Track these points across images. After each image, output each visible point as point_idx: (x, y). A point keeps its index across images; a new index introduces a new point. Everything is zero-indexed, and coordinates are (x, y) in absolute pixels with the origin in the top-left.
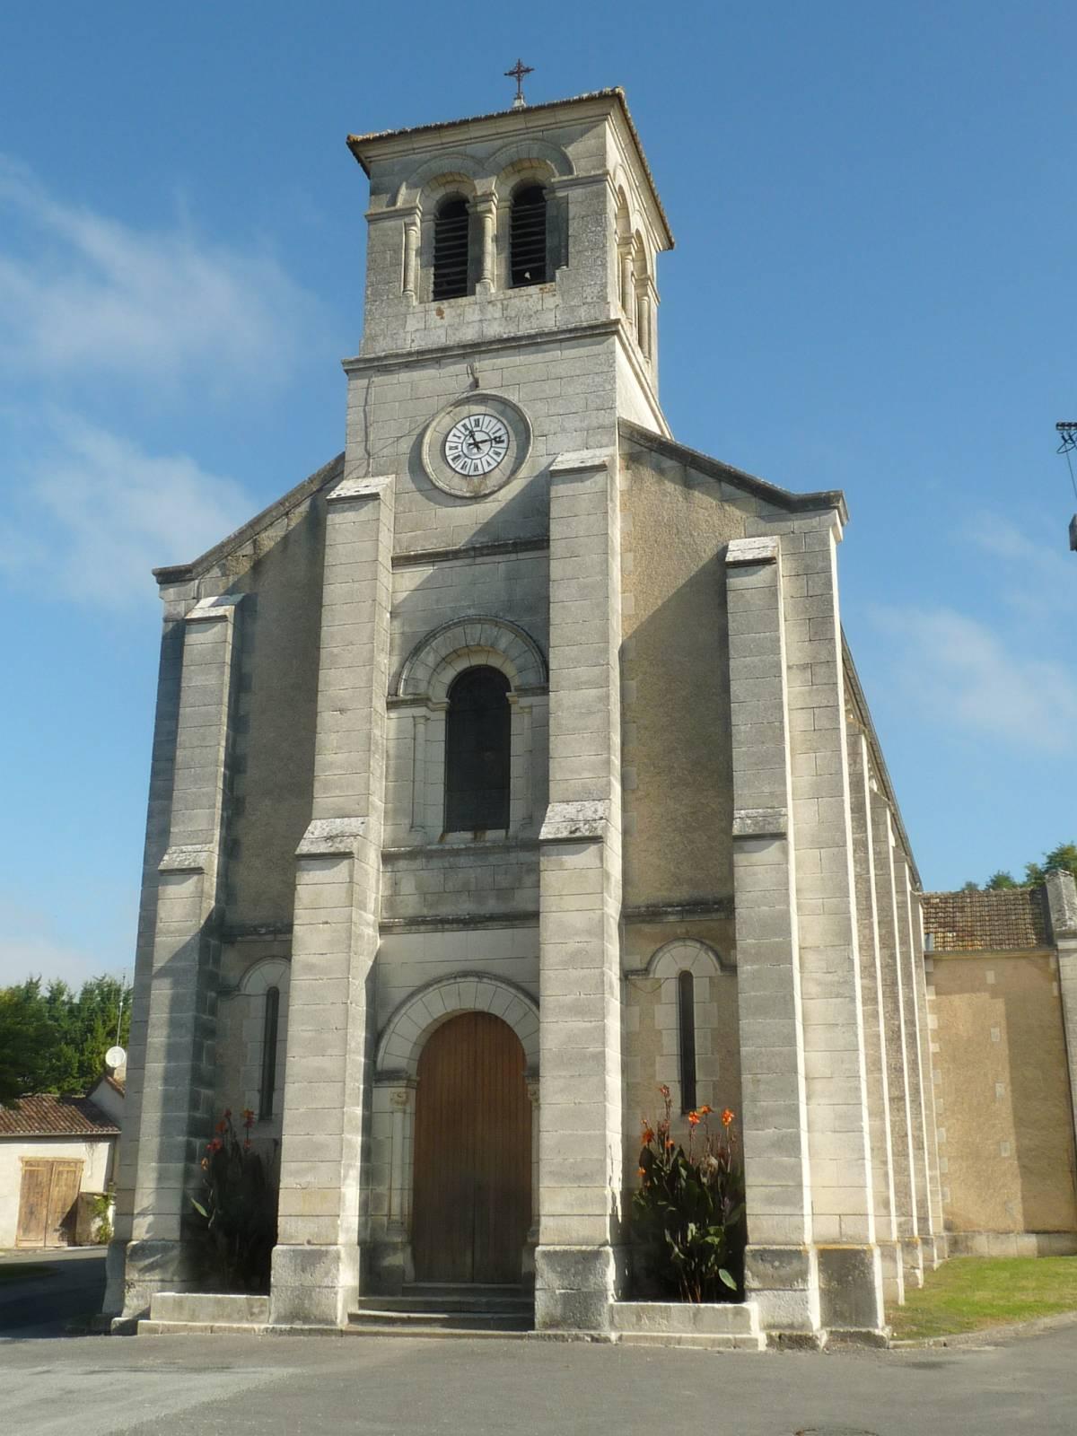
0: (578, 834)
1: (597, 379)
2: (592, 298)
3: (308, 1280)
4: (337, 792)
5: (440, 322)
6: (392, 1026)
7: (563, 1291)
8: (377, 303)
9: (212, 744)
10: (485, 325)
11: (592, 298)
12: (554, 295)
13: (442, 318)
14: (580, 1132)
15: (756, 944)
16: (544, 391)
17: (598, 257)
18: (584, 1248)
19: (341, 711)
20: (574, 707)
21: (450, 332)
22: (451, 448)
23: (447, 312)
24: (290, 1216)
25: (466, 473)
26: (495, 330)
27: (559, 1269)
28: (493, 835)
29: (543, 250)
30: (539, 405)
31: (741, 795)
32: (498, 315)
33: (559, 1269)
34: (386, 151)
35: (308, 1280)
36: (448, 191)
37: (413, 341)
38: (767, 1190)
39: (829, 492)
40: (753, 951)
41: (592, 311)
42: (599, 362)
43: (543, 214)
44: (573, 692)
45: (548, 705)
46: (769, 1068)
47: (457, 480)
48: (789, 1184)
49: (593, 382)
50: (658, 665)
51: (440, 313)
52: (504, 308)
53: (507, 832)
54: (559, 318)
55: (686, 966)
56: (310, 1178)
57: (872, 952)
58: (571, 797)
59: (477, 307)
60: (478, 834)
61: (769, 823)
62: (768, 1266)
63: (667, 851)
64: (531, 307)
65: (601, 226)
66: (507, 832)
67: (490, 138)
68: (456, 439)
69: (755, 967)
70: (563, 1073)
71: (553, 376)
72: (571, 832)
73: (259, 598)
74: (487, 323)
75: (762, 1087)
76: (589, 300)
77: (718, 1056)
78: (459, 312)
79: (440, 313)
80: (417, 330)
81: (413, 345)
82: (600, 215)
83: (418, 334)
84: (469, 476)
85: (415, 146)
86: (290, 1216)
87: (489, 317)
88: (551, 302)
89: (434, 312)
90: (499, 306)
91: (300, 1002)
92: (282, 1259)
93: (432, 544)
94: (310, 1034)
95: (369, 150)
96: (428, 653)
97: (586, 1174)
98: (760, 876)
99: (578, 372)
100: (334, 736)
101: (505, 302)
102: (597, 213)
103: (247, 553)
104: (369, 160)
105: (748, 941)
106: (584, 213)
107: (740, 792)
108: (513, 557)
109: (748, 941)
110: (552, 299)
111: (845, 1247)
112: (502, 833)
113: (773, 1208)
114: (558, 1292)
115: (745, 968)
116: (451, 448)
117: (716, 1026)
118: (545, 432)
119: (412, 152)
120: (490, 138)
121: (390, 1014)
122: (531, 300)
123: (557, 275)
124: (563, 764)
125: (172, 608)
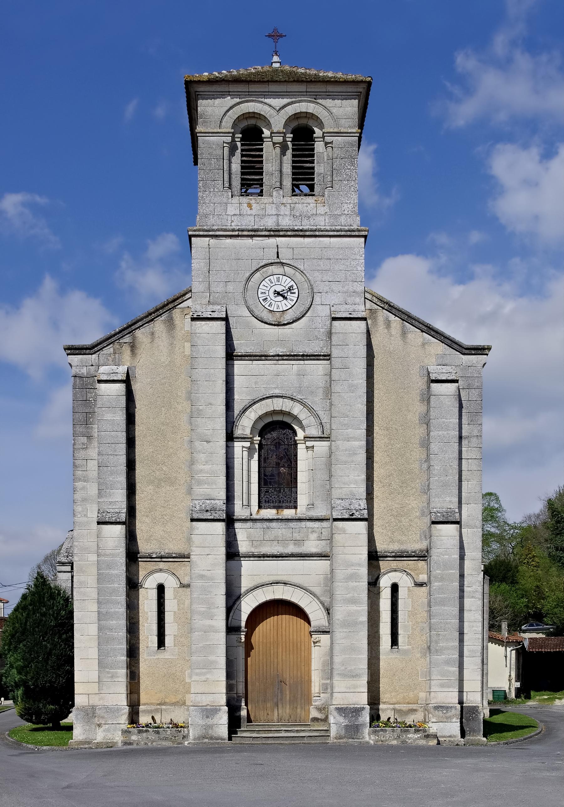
0: (354, 517)
1: (352, 263)
2: (348, 211)
3: (210, 721)
4: (206, 486)
5: (249, 212)
6: (236, 606)
7: (345, 724)
8: (207, 193)
9: (120, 454)
10: (280, 218)
11: (348, 211)
12: (324, 206)
13: (251, 209)
14: (354, 656)
15: (441, 573)
16: (319, 265)
17: (352, 186)
18: (356, 706)
19: (208, 442)
20: (346, 450)
21: (257, 219)
22: (262, 293)
23: (254, 206)
24: (198, 693)
25: (271, 309)
26: (286, 223)
27: (344, 715)
28: (288, 513)
29: (313, 174)
30: (317, 274)
31: (433, 501)
32: (288, 213)
33: (344, 715)
34: (211, 90)
35: (210, 721)
36: (249, 123)
37: (232, 221)
38: (441, 681)
39: (484, 346)
40: (439, 576)
41: (349, 220)
42: (354, 253)
43: (313, 150)
44: (345, 442)
45: (459, 481)
46: (444, 629)
47: (265, 312)
48: (452, 679)
49: (350, 264)
50: (384, 430)
51: (250, 206)
52: (292, 209)
53: (296, 511)
54: (327, 221)
55: (394, 581)
56: (208, 676)
57: (229, 551)
58: (344, 497)
59: (274, 206)
60: (280, 511)
61: (450, 516)
62: (440, 712)
63: (387, 526)
64: (309, 211)
65: (354, 166)
66: (296, 511)
67: (282, 94)
68: (265, 288)
69: (440, 584)
70: (345, 630)
71: (325, 258)
72: (350, 515)
73: (137, 369)
74: (281, 217)
75: (441, 637)
76: (346, 212)
77: (411, 623)
78: (262, 207)
79: (250, 206)
80: (234, 215)
81: (233, 224)
82: (354, 159)
83: (235, 217)
84: (273, 311)
85: (231, 90)
86: (198, 693)
87: (282, 213)
88: (322, 210)
89: (246, 205)
90: (288, 206)
91: (197, 593)
92: (194, 712)
93: (251, 349)
94: (204, 609)
95: (200, 87)
96: (251, 412)
97: (357, 675)
98: (444, 541)
99: (341, 257)
100: (202, 455)
101: (292, 205)
102: (352, 157)
103: (127, 341)
104: (198, 93)
105: (437, 571)
106: (343, 156)
107: (433, 500)
108: (302, 362)
109: (437, 571)
110: (322, 208)
111: (470, 705)
112: (293, 511)
113: (443, 689)
114: (343, 724)
115: (435, 584)
116: (262, 293)
117: (410, 610)
118: (321, 291)
119: (228, 93)
120: (282, 94)
121: (234, 600)
122: (309, 207)
123: (326, 193)
124: (339, 480)
125: (77, 370)
